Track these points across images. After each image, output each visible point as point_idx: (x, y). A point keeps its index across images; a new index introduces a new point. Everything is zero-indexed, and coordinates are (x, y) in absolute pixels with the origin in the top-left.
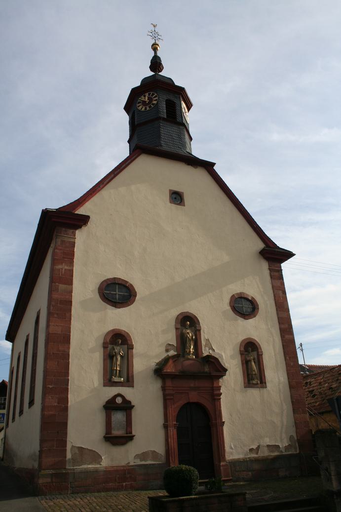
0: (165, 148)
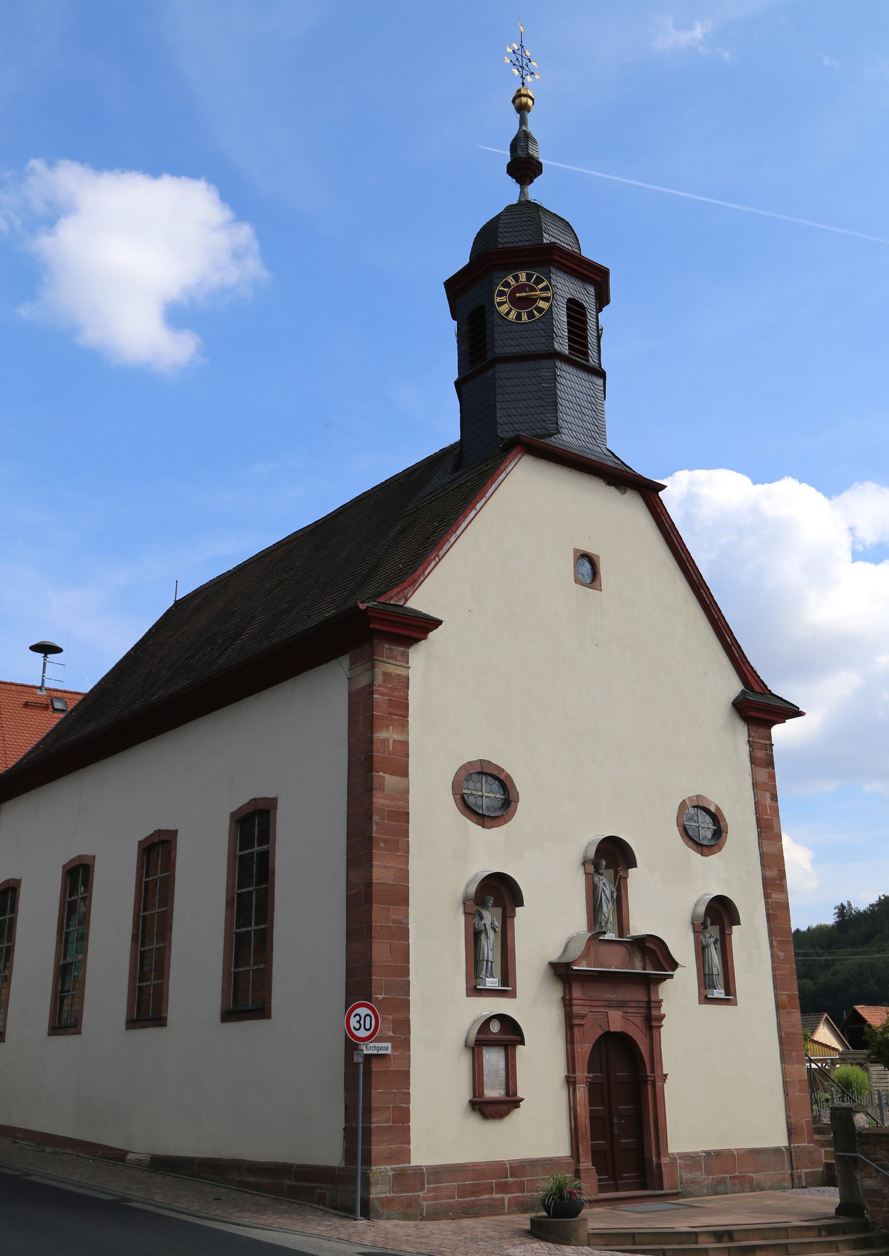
0: (569, 438)
